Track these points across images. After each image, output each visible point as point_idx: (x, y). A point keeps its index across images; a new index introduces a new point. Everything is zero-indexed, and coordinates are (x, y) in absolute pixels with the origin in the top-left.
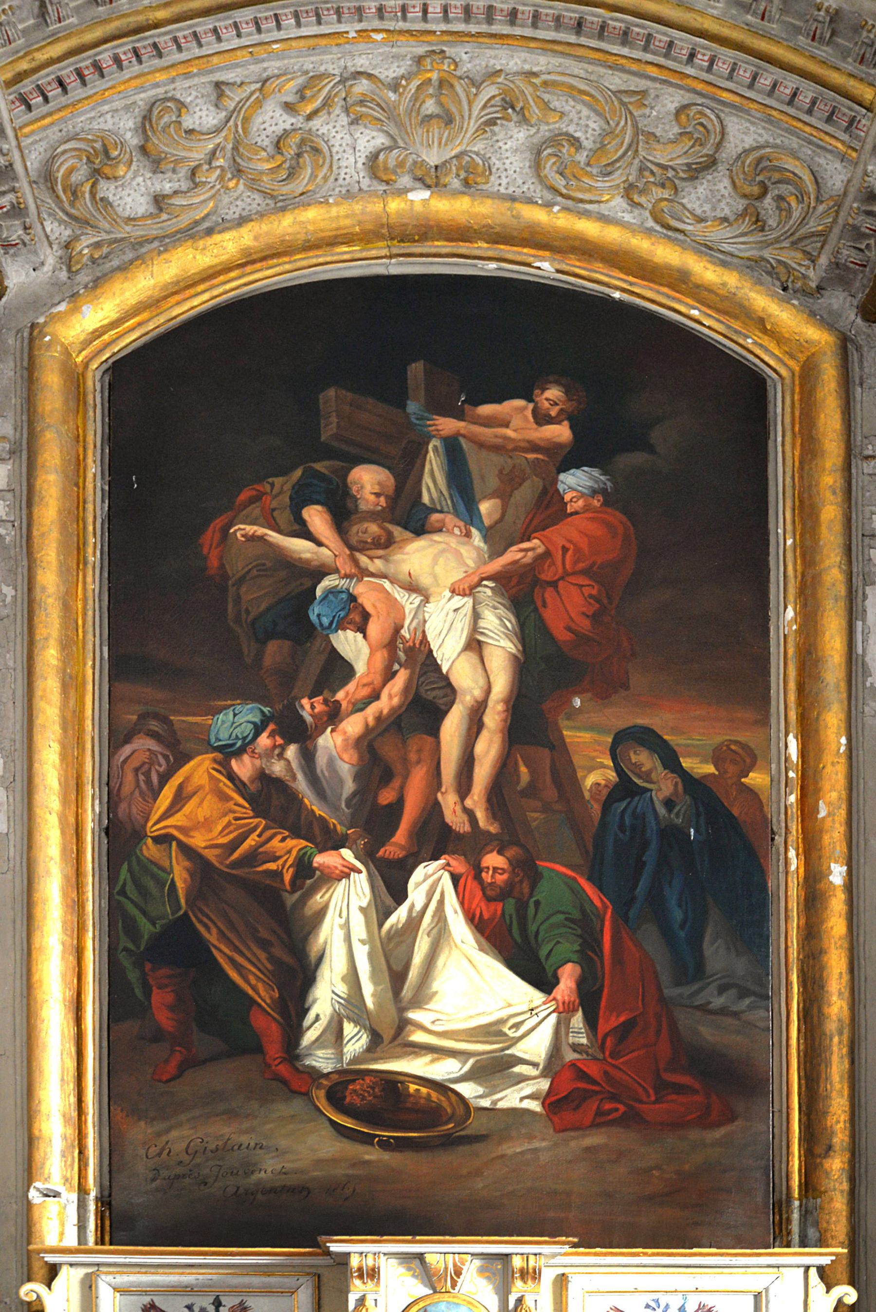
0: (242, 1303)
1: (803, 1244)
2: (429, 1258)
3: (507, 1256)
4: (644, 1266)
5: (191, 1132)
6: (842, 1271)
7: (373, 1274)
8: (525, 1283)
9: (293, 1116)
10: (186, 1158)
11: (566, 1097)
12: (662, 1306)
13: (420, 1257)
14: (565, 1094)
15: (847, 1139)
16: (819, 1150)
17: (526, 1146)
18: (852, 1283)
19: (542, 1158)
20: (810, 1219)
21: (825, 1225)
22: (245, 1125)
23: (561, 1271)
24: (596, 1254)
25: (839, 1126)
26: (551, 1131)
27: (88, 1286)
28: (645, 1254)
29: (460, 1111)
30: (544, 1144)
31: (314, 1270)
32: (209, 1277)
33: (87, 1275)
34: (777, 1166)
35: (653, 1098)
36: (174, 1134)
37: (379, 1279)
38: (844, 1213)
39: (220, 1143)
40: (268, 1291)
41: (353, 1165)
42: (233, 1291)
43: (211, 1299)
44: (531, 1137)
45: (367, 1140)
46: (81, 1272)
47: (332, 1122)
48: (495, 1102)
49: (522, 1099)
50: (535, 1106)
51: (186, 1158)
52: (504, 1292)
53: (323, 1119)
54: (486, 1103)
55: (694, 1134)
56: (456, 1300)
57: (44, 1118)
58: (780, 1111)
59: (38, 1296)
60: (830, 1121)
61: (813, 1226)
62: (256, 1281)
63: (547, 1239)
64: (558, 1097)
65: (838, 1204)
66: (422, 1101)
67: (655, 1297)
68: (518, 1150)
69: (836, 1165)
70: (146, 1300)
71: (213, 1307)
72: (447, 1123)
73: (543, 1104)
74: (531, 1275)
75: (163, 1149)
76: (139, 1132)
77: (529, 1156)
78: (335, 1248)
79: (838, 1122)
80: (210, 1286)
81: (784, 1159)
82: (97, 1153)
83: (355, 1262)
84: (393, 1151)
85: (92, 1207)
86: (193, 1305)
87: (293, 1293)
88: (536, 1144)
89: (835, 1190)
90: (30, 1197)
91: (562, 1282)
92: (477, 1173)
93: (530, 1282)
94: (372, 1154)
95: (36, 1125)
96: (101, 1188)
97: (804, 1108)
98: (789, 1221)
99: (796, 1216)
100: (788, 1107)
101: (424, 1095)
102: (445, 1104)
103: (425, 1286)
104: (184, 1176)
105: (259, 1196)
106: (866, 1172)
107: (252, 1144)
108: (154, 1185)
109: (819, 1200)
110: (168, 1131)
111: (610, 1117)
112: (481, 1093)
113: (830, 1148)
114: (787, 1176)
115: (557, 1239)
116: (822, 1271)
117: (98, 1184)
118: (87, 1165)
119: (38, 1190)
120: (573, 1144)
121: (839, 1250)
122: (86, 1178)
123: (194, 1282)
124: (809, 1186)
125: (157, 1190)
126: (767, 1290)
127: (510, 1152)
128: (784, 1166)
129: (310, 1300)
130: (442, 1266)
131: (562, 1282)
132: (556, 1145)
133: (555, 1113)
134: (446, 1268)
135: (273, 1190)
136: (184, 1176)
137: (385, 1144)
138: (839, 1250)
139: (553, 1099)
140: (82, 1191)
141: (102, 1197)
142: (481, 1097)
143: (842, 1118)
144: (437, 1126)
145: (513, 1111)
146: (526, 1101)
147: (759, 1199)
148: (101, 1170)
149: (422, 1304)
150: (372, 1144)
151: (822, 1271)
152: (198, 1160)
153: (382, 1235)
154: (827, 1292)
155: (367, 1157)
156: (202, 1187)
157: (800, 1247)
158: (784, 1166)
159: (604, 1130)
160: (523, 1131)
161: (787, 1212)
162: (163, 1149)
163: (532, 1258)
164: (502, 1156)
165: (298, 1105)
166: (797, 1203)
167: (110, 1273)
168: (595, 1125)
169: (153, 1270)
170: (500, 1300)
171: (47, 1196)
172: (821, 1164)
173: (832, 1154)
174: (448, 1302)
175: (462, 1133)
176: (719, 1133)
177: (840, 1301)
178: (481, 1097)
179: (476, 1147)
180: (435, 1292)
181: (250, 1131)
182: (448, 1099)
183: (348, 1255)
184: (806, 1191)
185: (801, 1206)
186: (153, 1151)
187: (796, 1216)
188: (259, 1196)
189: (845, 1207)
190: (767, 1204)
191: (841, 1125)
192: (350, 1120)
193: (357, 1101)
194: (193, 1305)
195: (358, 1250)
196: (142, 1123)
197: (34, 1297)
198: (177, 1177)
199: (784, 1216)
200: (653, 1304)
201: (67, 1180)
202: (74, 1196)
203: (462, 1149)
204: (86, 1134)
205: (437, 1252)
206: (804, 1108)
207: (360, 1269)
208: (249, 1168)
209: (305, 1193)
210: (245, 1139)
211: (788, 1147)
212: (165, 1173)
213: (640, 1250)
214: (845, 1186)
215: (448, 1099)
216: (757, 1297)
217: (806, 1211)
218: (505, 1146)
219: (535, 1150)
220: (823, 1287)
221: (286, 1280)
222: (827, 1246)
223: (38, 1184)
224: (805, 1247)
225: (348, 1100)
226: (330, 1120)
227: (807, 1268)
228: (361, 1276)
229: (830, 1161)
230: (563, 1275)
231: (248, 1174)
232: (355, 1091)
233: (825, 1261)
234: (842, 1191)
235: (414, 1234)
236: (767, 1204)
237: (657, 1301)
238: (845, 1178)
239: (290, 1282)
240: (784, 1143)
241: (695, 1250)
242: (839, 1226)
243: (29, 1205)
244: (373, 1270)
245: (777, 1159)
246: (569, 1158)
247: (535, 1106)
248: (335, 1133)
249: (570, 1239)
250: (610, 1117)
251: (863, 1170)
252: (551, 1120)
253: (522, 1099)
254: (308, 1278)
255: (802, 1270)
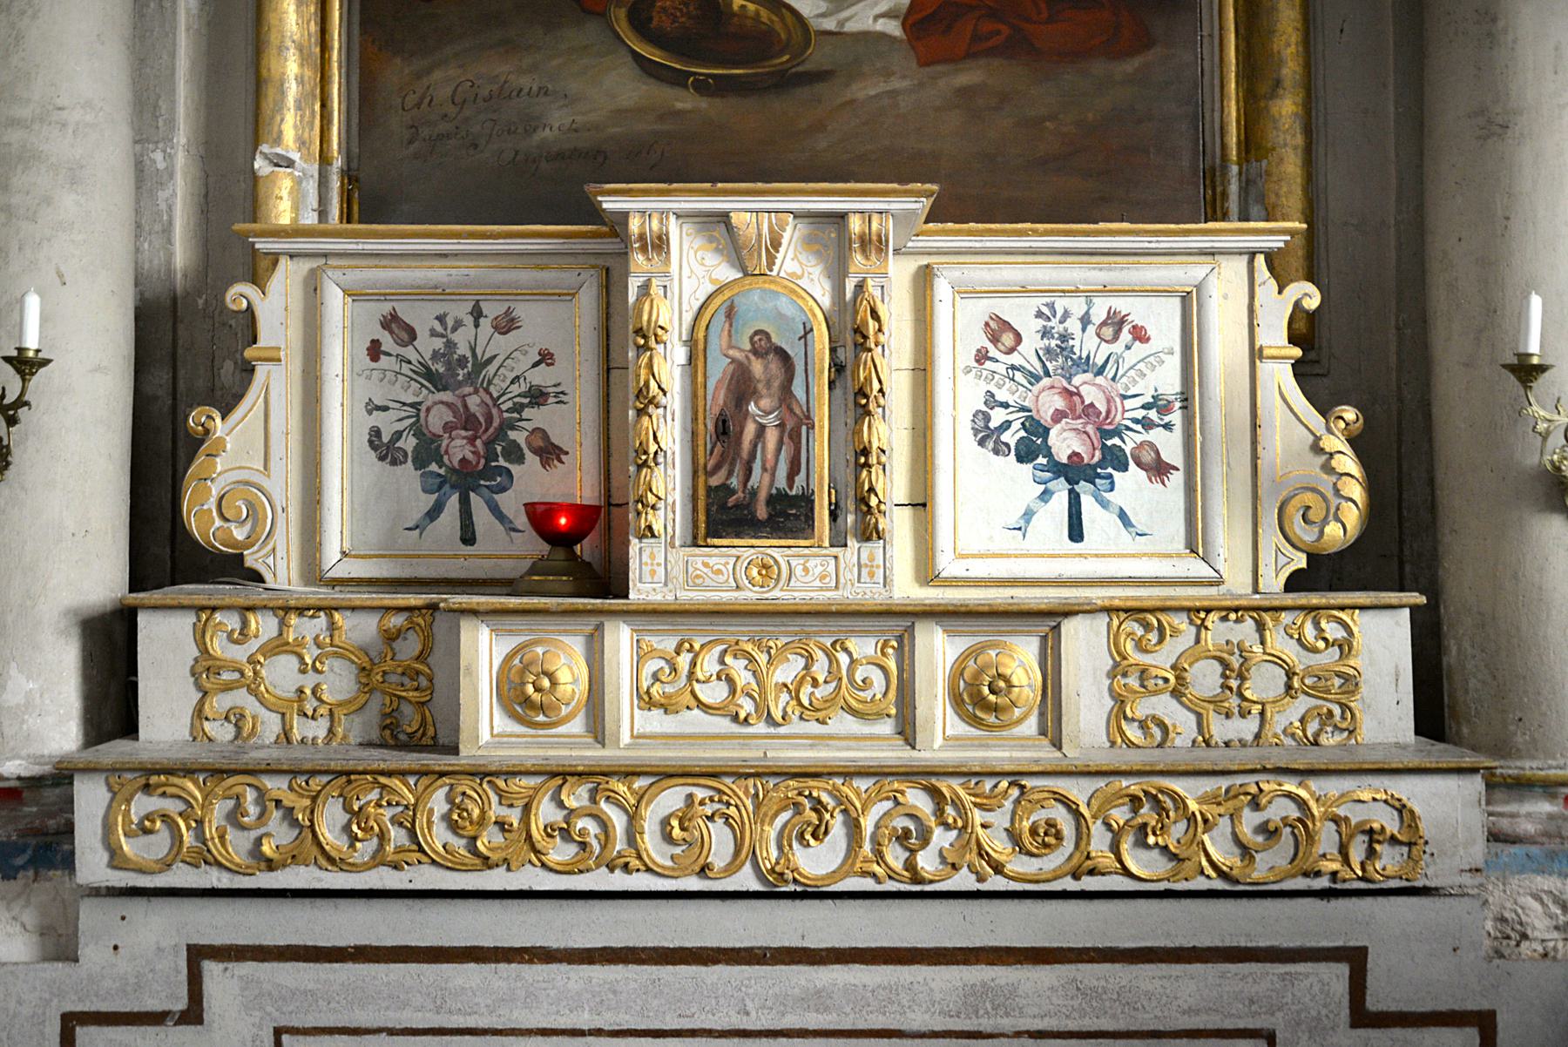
0: (508, 312)
1: (1244, 218)
2: (734, 218)
3: (842, 217)
4: (1034, 254)
5: (460, 71)
6: (1297, 262)
7: (660, 244)
8: (867, 258)
9: (586, 47)
10: (452, 110)
11: (933, 14)
12: (1059, 313)
13: (724, 218)
14: (930, 11)
15: (1299, 70)
16: (1263, 88)
17: (882, 87)
18: (1311, 277)
19: (902, 104)
20: (1253, 191)
21: (1273, 198)
22: (527, 61)
23: (924, 261)
24: (970, 233)
25: (1289, 51)
26: (914, 65)
27: (313, 289)
28: (1035, 232)
29: (797, 36)
30: (905, 84)
31: (600, 262)
32: (466, 271)
33: (313, 272)
34: (1207, 115)
35: (1045, 15)
36: (437, 75)
37: (668, 253)
38: (1299, 180)
39: (495, 87)
40: (540, 294)
41: (661, 118)
42: (497, 294)
43: (469, 306)
44: (888, 74)
45: (677, 79)
46: (305, 266)
47: (636, 56)
48: (841, 23)
49: (876, 18)
50: (893, 28)
51: (452, 110)
52: (838, 273)
53: (623, 51)
54: (830, 24)
55: (1099, 67)
56: (773, 287)
57: (274, 51)
58: (1211, 36)
59: (249, 306)
60: (1278, 44)
61: (1257, 202)
62: (526, 277)
63: (895, 186)
64: (924, 14)
65: (1291, 165)
66: (749, 23)
67: (1048, 300)
68: (872, 93)
69: (1286, 108)
70: (386, 308)
71: (471, 319)
72: (781, 53)
73: (903, 25)
74: (873, 244)
75: (422, 98)
76: (395, 72)
77: (886, 101)
78: (610, 204)
79: (1289, 45)
80: (466, 286)
81: (1217, 105)
82: (344, 107)
83: (634, 225)
84: (711, 95)
85: (335, 183)
86: (445, 315)
87: (573, 295)
88: (896, 84)
89: (1286, 145)
90: (256, 166)
91: (924, 280)
92: (819, 127)
93: (873, 257)
94: (686, 101)
95: (264, 62)
96: (349, 158)
97: (1242, 31)
98: (1225, 195)
99: (1234, 188)
100: (1221, 28)
101: (751, 14)
102: (778, 27)
103: (733, 266)
104: (448, 136)
105: (544, 165)
106: (1326, 124)
107: (535, 88)
108: (412, 148)
109: (1264, 163)
110: (429, 71)
111: (990, 44)
112: (823, 10)
113: (1278, 83)
114: (1222, 128)
115: (911, 186)
116: (1271, 258)
117: (344, 150)
118: (330, 122)
119: (266, 156)
120: (942, 83)
121: (1297, 225)
122: (329, 141)
123: (446, 279)
124: (1252, 144)
125: (416, 156)
126: (1199, 287)
127: (861, 95)
128: (1217, 115)
129: (595, 305)
130: (753, 231)
131: (924, 280)
132: (921, 85)
133: (918, 38)
134: (759, 235)
135: (560, 156)
136: (448, 136)
137: (702, 87)
138: (1297, 225)
139: (918, 17)
140: (324, 160)
141: (349, 169)
142: (823, 15)
143: (1293, 40)
144: (772, 57)
145: (865, 36)
146: (881, 21)
147: (1186, 163)
148: (348, 131)
149: (727, 294)
150: (685, 86)
151: (1271, 258)
152: (467, 112)
153: (671, 182)
154: (1280, 292)
155: (679, 105)
156: (472, 152)
157: (1240, 220)
158: (1217, 115)
159: (982, 62)
160: (878, 65)
161: (1223, 184)
162: (422, 98)
163: (875, 218)
164: (853, 101)
165: (592, 28)
166: (1235, 169)
167: (340, 267)
168: (970, 55)
169: (394, 263)
170: (833, 289)
171: (277, 165)
172: (1267, 108)
173: (1281, 92)
174: (764, 290)
175: (800, 69)
176: (1131, 65)
177: (1297, 304)
178: (823, 15)
179: (820, 88)
180: (746, 274)
181: (534, 68)
182: (782, 19)
183: (624, 216)
184: (1247, 152)
185: (1240, 173)
186: (411, 99)
187: (1234, 188)
188: (544, 165)
189: (1299, 171)
190: (1196, 173)
191: (1292, 49)
192: (657, 52)
193: (668, 25)
194: (445, 315)
195: (638, 207)
196: (398, 61)
197: (244, 304)
198: (441, 137)
199: (1219, 190)
200: (1046, 310)
201: (303, 143)
202: (314, 169)
203: (803, 93)
204: (330, 77)
205: (748, 210)
206: (1242, 31)
207: (642, 237)
208: (531, 124)
209: (600, 159)
210: (525, 82)
211: (1222, 87)
212: (425, 132)
213: (1028, 225)
214: (1299, 140)
215: (782, 19)
216: (1186, 299)
217: (1248, 182)
218: (854, 87)
219: (893, 94)
220: (1273, 283)
221: (564, 275)
222: (1276, 220)
223: (265, 148)
224: (1247, 220)
225: (655, 23)
226: (633, 52)
227: (1252, 255)
228: (644, 249)
229: (1278, 102)
230: (927, 266)
231: (530, 130)
232: (664, 9)
233: (1277, 242)
234: (1295, 148)
235: (714, 181)
236: (1196, 173)
237: (1051, 306)
238: (1298, 128)
239: (568, 278)
240: (1217, 82)
241: (1102, 225)
242: (1292, 196)
243: (254, 177)
244: (660, 238)
245: (1207, 106)
246: (938, 103)
247: (893, 28)
248: (638, 71)
249: (928, 186)
250: (990, 44)
251: (1321, 120)
252: (913, 48)
253: (876, 18)
254: (592, 272)
255: (1245, 258)
